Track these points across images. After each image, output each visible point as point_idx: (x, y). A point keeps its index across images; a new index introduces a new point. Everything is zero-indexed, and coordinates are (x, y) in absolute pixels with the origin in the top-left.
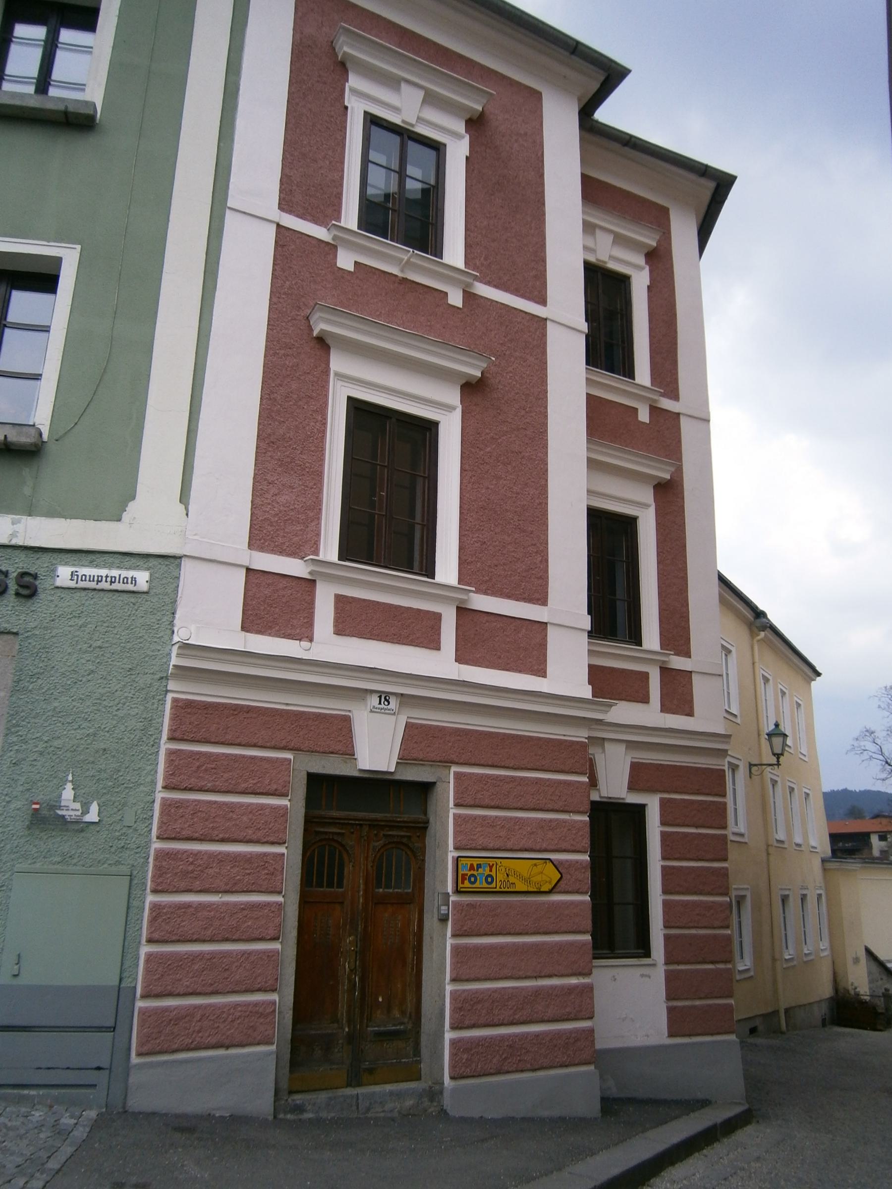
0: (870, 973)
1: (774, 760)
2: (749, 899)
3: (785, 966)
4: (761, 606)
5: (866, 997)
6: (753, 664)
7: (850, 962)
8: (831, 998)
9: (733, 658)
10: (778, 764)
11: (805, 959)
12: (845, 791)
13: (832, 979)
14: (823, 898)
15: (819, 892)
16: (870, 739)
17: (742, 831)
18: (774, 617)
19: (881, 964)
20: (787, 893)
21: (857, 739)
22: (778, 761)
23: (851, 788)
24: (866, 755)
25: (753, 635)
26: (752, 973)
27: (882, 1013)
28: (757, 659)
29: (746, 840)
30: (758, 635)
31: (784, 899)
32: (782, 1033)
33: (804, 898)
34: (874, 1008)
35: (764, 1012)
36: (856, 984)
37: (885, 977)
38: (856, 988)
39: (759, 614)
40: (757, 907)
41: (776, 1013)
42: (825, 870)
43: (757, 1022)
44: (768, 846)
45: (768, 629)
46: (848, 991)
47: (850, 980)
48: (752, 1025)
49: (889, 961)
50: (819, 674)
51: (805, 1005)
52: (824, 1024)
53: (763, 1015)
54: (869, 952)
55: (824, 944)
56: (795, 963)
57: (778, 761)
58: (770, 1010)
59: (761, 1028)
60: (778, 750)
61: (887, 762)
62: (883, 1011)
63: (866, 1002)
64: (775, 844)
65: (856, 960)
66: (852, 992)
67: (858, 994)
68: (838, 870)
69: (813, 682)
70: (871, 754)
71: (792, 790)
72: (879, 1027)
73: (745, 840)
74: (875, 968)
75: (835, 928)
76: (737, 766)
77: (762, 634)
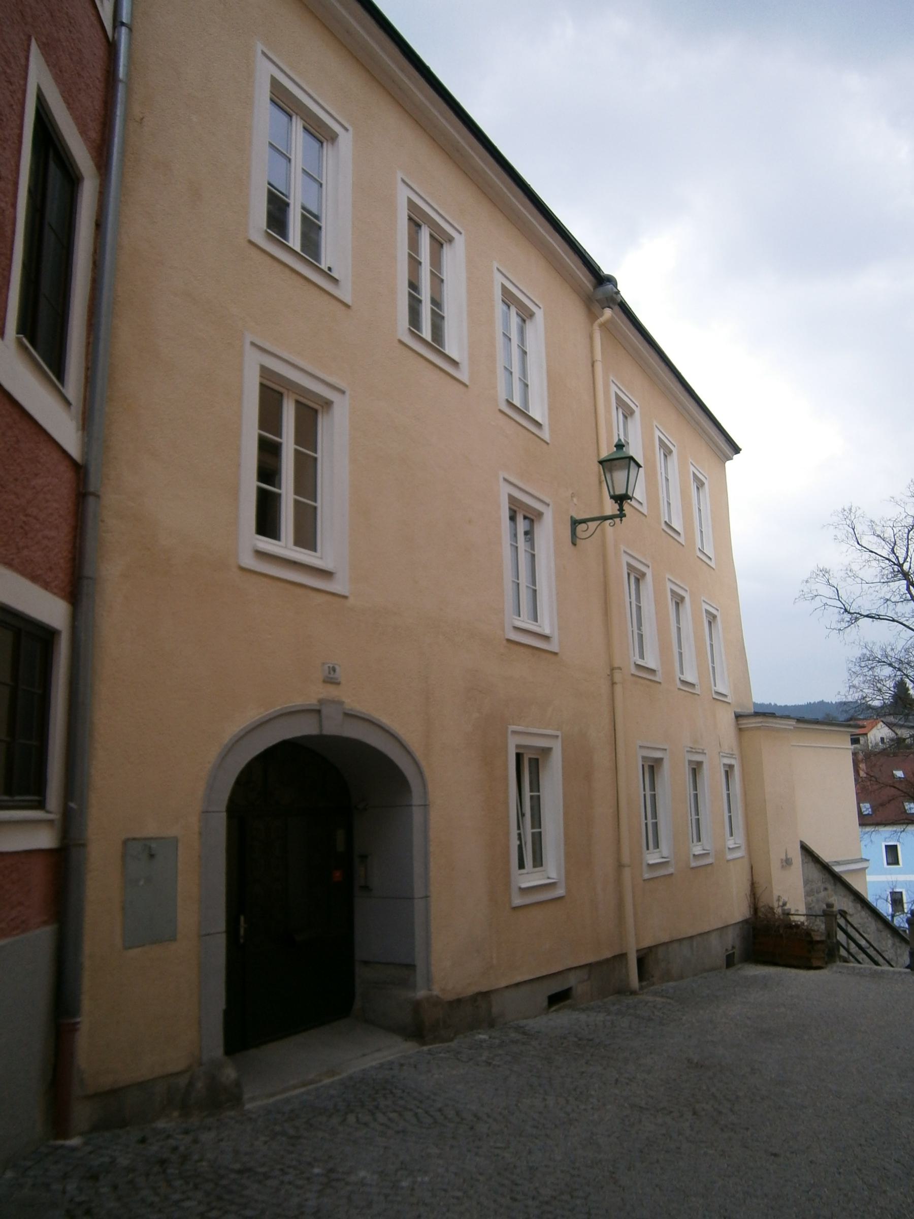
0: (807, 882)
1: (610, 507)
2: (557, 757)
3: (646, 876)
4: (606, 270)
5: (796, 918)
6: (593, 366)
7: (775, 866)
8: (746, 922)
9: (536, 331)
10: (621, 515)
11: (693, 864)
12: (822, 703)
13: (748, 892)
14: (737, 771)
15: (727, 761)
16: (824, 580)
17: (547, 631)
18: (628, 292)
19: (826, 868)
20: (658, 755)
21: (807, 582)
22: (621, 509)
23: (826, 701)
24: (818, 602)
25: (592, 317)
26: (560, 892)
27: (818, 942)
28: (598, 356)
29: (556, 650)
30: (602, 315)
31: (652, 768)
32: (633, 993)
33: (696, 769)
34: (808, 933)
35: (591, 959)
36: (785, 898)
37: (830, 887)
38: (785, 904)
39: (601, 280)
40: (579, 771)
41: (621, 957)
42: (740, 730)
43: (572, 981)
44: (613, 669)
45: (617, 308)
46: (772, 909)
47: (776, 893)
48: (556, 987)
49: (838, 863)
50: (737, 450)
51: (691, 937)
52: (730, 962)
53: (589, 967)
54: (806, 851)
55: (736, 841)
56: (671, 870)
57: (621, 509)
58: (607, 954)
59: (580, 989)
60: (620, 491)
61: (846, 610)
62: (823, 938)
63: (797, 926)
64: (633, 670)
65: (787, 862)
66: (779, 911)
67: (788, 914)
68: (758, 728)
69: (728, 464)
70: (825, 600)
71: (679, 601)
72: (816, 963)
73: (554, 647)
74: (815, 873)
75: (754, 817)
76: (540, 515)
77: (608, 313)
